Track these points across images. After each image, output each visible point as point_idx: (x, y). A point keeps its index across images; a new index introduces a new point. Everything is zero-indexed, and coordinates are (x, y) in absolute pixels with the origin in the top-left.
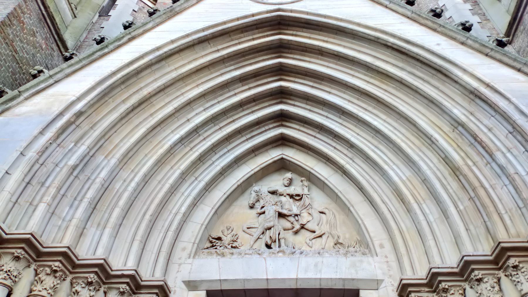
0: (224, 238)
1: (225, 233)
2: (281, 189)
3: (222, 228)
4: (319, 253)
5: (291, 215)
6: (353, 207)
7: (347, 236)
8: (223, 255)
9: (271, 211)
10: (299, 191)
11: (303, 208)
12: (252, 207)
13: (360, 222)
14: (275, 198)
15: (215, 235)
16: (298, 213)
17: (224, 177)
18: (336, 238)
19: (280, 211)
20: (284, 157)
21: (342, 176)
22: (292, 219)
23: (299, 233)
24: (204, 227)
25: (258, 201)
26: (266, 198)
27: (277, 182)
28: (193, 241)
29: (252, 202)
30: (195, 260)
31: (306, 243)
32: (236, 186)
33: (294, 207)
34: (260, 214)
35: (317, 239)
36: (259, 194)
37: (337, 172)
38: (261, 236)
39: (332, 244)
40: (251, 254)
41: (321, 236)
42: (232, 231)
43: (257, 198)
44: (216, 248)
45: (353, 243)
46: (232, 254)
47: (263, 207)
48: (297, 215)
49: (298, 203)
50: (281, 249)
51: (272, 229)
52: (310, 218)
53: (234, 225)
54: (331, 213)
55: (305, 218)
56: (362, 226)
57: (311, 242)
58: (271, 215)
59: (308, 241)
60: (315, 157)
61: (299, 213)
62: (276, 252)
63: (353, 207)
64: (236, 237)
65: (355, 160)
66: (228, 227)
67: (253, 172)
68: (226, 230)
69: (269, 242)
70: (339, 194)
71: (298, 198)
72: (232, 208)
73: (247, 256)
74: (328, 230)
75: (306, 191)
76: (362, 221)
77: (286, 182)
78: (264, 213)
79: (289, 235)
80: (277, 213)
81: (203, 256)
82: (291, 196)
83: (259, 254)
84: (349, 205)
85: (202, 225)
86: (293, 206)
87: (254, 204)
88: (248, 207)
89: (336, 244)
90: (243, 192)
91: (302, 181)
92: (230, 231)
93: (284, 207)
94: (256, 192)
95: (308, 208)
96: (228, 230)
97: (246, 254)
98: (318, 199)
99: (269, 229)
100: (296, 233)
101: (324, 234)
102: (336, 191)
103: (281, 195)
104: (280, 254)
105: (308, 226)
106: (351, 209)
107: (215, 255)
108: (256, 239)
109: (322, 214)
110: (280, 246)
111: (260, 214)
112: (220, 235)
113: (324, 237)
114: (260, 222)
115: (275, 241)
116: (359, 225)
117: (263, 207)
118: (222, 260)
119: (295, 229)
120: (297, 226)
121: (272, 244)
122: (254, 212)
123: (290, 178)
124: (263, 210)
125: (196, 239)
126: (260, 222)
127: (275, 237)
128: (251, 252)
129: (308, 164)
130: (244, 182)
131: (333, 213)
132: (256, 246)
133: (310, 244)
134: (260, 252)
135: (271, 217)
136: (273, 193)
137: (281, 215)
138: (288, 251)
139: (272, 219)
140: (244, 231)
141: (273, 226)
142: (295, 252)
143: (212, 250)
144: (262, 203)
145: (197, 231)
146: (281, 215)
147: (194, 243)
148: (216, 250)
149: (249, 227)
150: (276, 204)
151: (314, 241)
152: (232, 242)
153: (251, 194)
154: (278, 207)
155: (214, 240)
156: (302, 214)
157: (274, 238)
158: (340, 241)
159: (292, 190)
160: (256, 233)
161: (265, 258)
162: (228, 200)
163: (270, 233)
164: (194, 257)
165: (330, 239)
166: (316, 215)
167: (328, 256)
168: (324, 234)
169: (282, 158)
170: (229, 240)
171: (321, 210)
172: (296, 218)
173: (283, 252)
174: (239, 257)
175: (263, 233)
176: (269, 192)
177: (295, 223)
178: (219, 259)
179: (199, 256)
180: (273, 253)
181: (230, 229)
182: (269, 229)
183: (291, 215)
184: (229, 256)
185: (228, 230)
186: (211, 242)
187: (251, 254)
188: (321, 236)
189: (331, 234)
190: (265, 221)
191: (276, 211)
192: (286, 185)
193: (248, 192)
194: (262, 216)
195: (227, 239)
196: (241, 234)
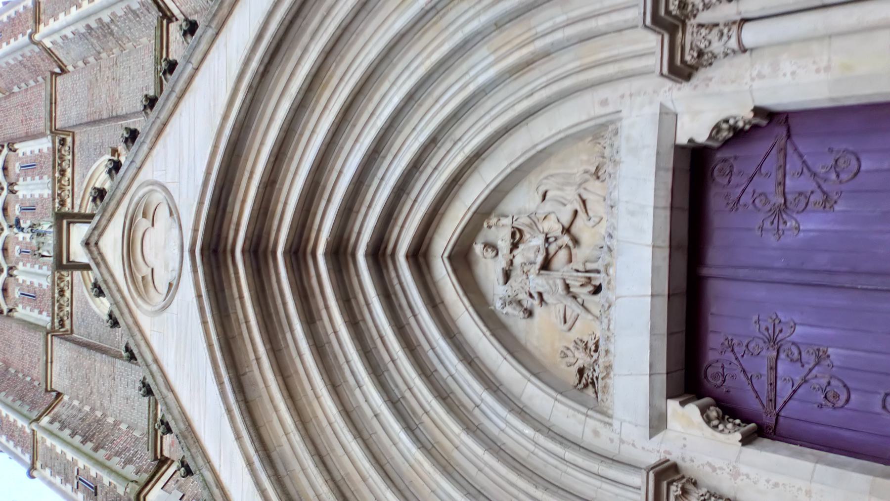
0: (580, 364)
1: (573, 360)
2: (502, 262)
3: (563, 366)
4: (612, 207)
6: (537, 145)
7: (584, 157)
8: (608, 368)
9: (537, 283)
10: (506, 233)
12: (530, 313)
14: (516, 274)
15: (574, 379)
17: (477, 357)
18: (587, 176)
19: (538, 266)
20: (446, 254)
21: (484, 160)
22: (553, 248)
24: (559, 397)
25: (519, 303)
27: (489, 270)
29: (522, 313)
30: (615, 416)
31: (593, 227)
33: (534, 242)
34: (542, 300)
38: (580, 300)
39: (597, 183)
40: (609, 321)
41: (584, 202)
42: (568, 349)
43: (514, 305)
44: (597, 378)
47: (531, 295)
49: (527, 236)
50: (602, 269)
51: (568, 282)
52: (553, 217)
53: (560, 346)
54: (545, 181)
55: (552, 226)
57: (593, 219)
58: (544, 282)
59: (591, 223)
61: (544, 236)
62: (607, 279)
63: (537, 145)
64: (579, 342)
67: (471, 309)
71: (518, 236)
72: (530, 347)
73: (611, 327)
75: (506, 221)
77: (490, 253)
79: (580, 254)
80: (542, 272)
82: (515, 246)
83: (609, 307)
84: (533, 152)
85: (556, 400)
87: (526, 309)
88: (529, 320)
89: (598, 178)
91: (489, 227)
94: (504, 305)
96: (566, 356)
97: (608, 329)
98: (522, 202)
99: (567, 287)
100: (576, 242)
101: (580, 196)
102: (509, 170)
104: (611, 271)
107: (608, 381)
109: (547, 197)
111: (542, 300)
112: (575, 369)
113: (585, 197)
114: (555, 302)
115: (590, 278)
117: (531, 295)
118: (616, 369)
119: (571, 244)
120: (566, 239)
121: (594, 283)
122: (538, 311)
123: (482, 246)
124: (536, 296)
125: (579, 412)
126: (555, 302)
131: (546, 178)
132: (595, 310)
134: (607, 305)
135: (548, 283)
136: (507, 276)
137: (546, 265)
138: (608, 259)
140: (570, 329)
141: (564, 280)
143: (600, 385)
144: (523, 296)
145: (566, 409)
146: (546, 265)
147: (587, 416)
150: (526, 273)
151: (591, 214)
152: (588, 351)
153: (507, 314)
154: (532, 271)
155: (584, 381)
156: (546, 230)
157: (584, 281)
158: (593, 169)
159: (504, 245)
160: (573, 308)
161: (617, 298)
162: (516, 354)
163: (575, 286)
164: (610, 417)
165: (587, 185)
166: (548, 207)
168: (580, 196)
170: (583, 354)
171: (539, 198)
173: (607, 266)
176: (506, 283)
177: (559, 242)
178: (615, 375)
179: (609, 408)
180: (609, 283)
181: (566, 352)
182: (567, 287)
184: (611, 358)
185: (566, 356)
186: (586, 386)
187: (609, 321)
188: (584, 202)
189: (580, 185)
190: (554, 293)
191: (538, 274)
192: (494, 253)
193: (504, 318)
194: (545, 297)
195: (583, 359)
196: (575, 334)
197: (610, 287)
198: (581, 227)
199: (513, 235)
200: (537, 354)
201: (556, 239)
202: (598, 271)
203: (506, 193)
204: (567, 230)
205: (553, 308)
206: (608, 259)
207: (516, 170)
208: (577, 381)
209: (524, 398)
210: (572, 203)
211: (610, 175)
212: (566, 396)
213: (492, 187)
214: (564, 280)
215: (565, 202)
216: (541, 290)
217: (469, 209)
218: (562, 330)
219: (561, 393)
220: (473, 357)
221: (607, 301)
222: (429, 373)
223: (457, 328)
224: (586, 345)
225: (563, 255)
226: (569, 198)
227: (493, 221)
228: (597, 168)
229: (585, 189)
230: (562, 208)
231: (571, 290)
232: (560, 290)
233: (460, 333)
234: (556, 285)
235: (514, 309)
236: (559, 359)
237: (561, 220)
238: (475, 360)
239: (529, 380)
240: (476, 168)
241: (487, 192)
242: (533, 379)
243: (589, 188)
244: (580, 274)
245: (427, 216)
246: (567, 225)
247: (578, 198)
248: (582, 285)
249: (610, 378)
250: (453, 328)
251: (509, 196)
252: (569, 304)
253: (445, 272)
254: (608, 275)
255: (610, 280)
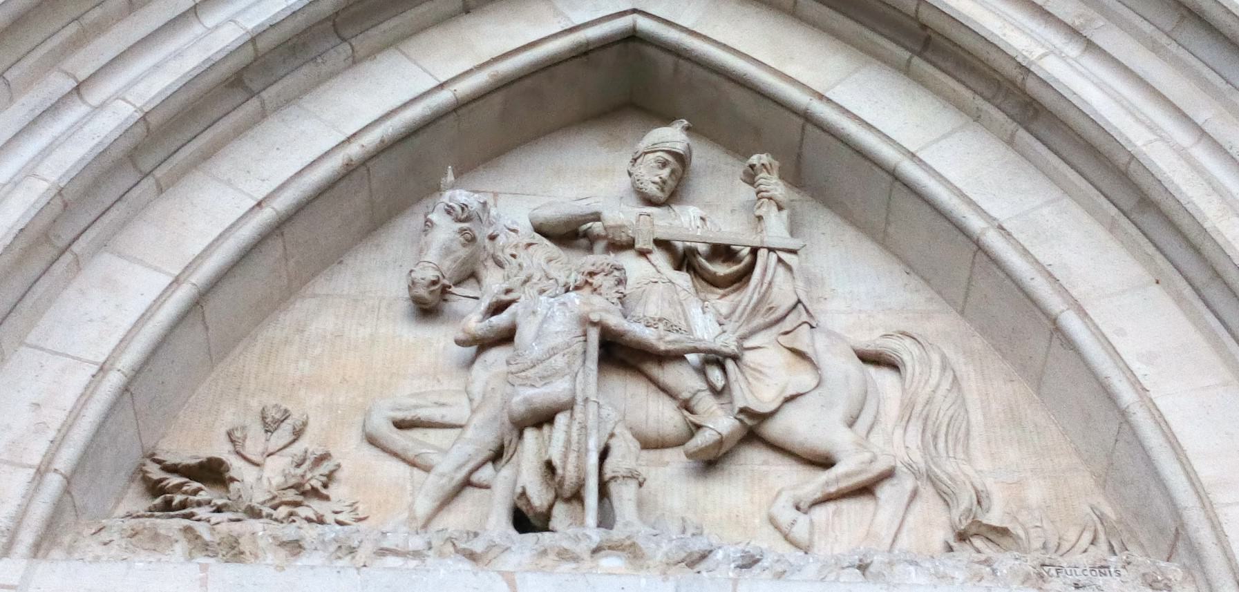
0: (237, 467)
1: (253, 448)
2: (620, 213)
3: (229, 417)
4: (863, 567)
5: (677, 357)
6: (1082, 313)
7: (1035, 493)
8: (233, 551)
9: (553, 321)
10: (729, 228)
11: (759, 321)
12: (428, 308)
13: (1127, 396)
14: (573, 263)
15: (186, 448)
16: (727, 343)
17: (263, 115)
18: (966, 499)
19: (615, 321)
20: (644, 24)
21: (1010, 142)
22: (682, 378)
23: (731, 467)
24: (114, 380)
25: (470, 275)
26: (523, 257)
27: (594, 177)
28: (36, 460)
29: (431, 275)
30: (42, 567)
31: (772, 521)
32: (334, 164)
33: (704, 320)
34: (483, 344)
35: (847, 506)
36: (482, 233)
37: (977, 117)
38: (486, 473)
39: (941, 535)
40: (417, 554)
41: (865, 490)
42: (298, 434)
43: (463, 252)
44: (190, 516)
45: (1072, 535)
46: (295, 547)
47: (498, 308)
48: (716, 359)
49: (722, 302)
50: (617, 534)
51: (561, 419)
52: (803, 378)
53: (307, 405)
54: (936, 359)
55: (766, 377)
56: (1141, 418)
57: (803, 519)
58: (559, 340)
59: (786, 514)
60: (836, 34)
61: (732, 347)
62: (583, 548)
63: (1082, 313)
64: (325, 468)
65: (1099, 39)
66: (273, 414)
67: (445, 97)
68: (256, 429)
69: (539, 497)
70: (993, 240)
71: (721, 269)
72: (301, 308)
73: (391, 561)
74: (917, 457)
75: (776, 229)
76: (1135, 382)
77: (651, 176)
78: (506, 337)
79: (668, 474)
80: (594, 335)
81: (99, 550)
82: (684, 260)
83: (472, 556)
84: (1054, 303)
85: (103, 369)
86: (695, 311)
87: (445, 290)
88: (404, 305)
89: (962, 537)
90: (376, 221)
91: (751, 177)
92: (283, 435)
93: (639, 311)
94: (463, 215)
95: (787, 325)
96: (270, 426)
97: (383, 552)
98: (849, 286)
99: (543, 419)
100: (711, 462)
101: (888, 475)
102: (975, 223)
103: (617, 246)
104: (610, 562)
105: (785, 427)
106: (1072, 323)
107: (181, 548)
108: (448, 484)
109: (871, 370)
110: (606, 519)
111: (483, 344)
112: (221, 450)
113: (885, 492)
114: (477, 389)
115: (577, 497)
116: (1124, 415)
117: (498, 308)
118: (224, 573)
119: (702, 439)
120: (720, 422)
121: (560, 510)
122: (439, 340)
123: (680, 148)
124: (501, 320)
125: (56, 445)
126: (477, 389)
127: (581, 468)
128: (417, 543)
129: (790, 70)
130: (386, 148)
131: (945, 365)
132: (456, 519)
133: (801, 531)
134: (478, 546)
135: (553, 352)
136: (568, 234)
137: (620, 354)
138: (659, 551)
139: (559, 361)
140: (372, 441)
141: (569, 406)
142: (703, 556)
143: (172, 525)
144: (494, 283)
145: (69, 398)
146: (620, 354)
147: (41, 472)
148: (186, 522)
149: (408, 415)
150: (587, 283)
151: (821, 513)
152: (291, 495)
153: (429, 224)
154: (597, 300)
155: (175, 480)
156: (749, 357)
157: (569, 473)
158: (994, 518)
159: (686, 223)
160: (450, 454)
161: (509, 578)
162: (275, 249)
163: (546, 444)
164: (37, 549)
165: (929, 504)
166: (841, 367)
167: (923, 580)
168: (888, 475)
169: (632, 37)
170: (278, 480)
171: (870, 340)
172: (715, 375)
173: (631, 551)
174: (346, 561)
175: (497, 456)
176: (540, 230)
177: (706, 403)
178: (204, 568)
179: (70, 550)
180: (564, 555)
181: (286, 428)
182: (543, 419)
183: (677, 357)
184: (273, 557)
185: (270, 426)
186: (155, 488)
187: (417, 554)
188: (865, 490)
189: (932, 480)
190: (513, 378)
191: (587, 322)
192: (652, 190)
193: (411, 223)
194: (497, 355)
195: (256, 480)
196: (352, 455)
197: (550, 559)
198: (762, 483)
199: (723, 252)
200: (275, 331)
201: (717, 393)
202: (606, 519)
203: (879, 233)
204: (754, 431)
205: (452, 384)
206: (659, 551)
207: (979, 247)
208: (171, 460)
209: (107, 263)
210: (862, 445)
211: (987, 562)
212: (114, 407)
213: (909, 170)
214: (569, 406)
215: (863, 424)
216: (525, 334)
217: (821, 97)
218: (367, 414)
219: (126, 389)
220: (269, 94)
221: (491, 546)
222: (147, 163)
223: (373, 53)
224: (315, 493)
225: (662, 415)
226: (876, 439)
227: (775, 186)
228: (1004, 532)
229: (915, 494)
230: (840, 411)
231: (530, 434)
232: (530, 392)
233: (355, 61)
234: (546, 379)
235: (447, 251)
236: (255, 404)
237: (790, 408)
238: (253, 105)
239: (177, 281)
240: (977, 117)
241: (887, 153)
242: (184, 294)
243: (918, 506)
244: (593, 459)
245: (639, 343)
246: (773, 429)
247: (880, 467)
248: (550, 467)
249: (190, 557)
250: (376, 34)
251: (869, 249)
252: (469, 433)
253: (578, 19)
254: (596, 551)
255: (576, 559)
